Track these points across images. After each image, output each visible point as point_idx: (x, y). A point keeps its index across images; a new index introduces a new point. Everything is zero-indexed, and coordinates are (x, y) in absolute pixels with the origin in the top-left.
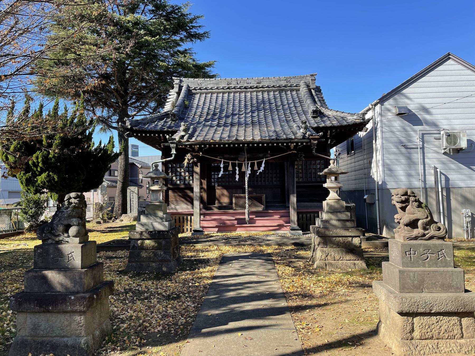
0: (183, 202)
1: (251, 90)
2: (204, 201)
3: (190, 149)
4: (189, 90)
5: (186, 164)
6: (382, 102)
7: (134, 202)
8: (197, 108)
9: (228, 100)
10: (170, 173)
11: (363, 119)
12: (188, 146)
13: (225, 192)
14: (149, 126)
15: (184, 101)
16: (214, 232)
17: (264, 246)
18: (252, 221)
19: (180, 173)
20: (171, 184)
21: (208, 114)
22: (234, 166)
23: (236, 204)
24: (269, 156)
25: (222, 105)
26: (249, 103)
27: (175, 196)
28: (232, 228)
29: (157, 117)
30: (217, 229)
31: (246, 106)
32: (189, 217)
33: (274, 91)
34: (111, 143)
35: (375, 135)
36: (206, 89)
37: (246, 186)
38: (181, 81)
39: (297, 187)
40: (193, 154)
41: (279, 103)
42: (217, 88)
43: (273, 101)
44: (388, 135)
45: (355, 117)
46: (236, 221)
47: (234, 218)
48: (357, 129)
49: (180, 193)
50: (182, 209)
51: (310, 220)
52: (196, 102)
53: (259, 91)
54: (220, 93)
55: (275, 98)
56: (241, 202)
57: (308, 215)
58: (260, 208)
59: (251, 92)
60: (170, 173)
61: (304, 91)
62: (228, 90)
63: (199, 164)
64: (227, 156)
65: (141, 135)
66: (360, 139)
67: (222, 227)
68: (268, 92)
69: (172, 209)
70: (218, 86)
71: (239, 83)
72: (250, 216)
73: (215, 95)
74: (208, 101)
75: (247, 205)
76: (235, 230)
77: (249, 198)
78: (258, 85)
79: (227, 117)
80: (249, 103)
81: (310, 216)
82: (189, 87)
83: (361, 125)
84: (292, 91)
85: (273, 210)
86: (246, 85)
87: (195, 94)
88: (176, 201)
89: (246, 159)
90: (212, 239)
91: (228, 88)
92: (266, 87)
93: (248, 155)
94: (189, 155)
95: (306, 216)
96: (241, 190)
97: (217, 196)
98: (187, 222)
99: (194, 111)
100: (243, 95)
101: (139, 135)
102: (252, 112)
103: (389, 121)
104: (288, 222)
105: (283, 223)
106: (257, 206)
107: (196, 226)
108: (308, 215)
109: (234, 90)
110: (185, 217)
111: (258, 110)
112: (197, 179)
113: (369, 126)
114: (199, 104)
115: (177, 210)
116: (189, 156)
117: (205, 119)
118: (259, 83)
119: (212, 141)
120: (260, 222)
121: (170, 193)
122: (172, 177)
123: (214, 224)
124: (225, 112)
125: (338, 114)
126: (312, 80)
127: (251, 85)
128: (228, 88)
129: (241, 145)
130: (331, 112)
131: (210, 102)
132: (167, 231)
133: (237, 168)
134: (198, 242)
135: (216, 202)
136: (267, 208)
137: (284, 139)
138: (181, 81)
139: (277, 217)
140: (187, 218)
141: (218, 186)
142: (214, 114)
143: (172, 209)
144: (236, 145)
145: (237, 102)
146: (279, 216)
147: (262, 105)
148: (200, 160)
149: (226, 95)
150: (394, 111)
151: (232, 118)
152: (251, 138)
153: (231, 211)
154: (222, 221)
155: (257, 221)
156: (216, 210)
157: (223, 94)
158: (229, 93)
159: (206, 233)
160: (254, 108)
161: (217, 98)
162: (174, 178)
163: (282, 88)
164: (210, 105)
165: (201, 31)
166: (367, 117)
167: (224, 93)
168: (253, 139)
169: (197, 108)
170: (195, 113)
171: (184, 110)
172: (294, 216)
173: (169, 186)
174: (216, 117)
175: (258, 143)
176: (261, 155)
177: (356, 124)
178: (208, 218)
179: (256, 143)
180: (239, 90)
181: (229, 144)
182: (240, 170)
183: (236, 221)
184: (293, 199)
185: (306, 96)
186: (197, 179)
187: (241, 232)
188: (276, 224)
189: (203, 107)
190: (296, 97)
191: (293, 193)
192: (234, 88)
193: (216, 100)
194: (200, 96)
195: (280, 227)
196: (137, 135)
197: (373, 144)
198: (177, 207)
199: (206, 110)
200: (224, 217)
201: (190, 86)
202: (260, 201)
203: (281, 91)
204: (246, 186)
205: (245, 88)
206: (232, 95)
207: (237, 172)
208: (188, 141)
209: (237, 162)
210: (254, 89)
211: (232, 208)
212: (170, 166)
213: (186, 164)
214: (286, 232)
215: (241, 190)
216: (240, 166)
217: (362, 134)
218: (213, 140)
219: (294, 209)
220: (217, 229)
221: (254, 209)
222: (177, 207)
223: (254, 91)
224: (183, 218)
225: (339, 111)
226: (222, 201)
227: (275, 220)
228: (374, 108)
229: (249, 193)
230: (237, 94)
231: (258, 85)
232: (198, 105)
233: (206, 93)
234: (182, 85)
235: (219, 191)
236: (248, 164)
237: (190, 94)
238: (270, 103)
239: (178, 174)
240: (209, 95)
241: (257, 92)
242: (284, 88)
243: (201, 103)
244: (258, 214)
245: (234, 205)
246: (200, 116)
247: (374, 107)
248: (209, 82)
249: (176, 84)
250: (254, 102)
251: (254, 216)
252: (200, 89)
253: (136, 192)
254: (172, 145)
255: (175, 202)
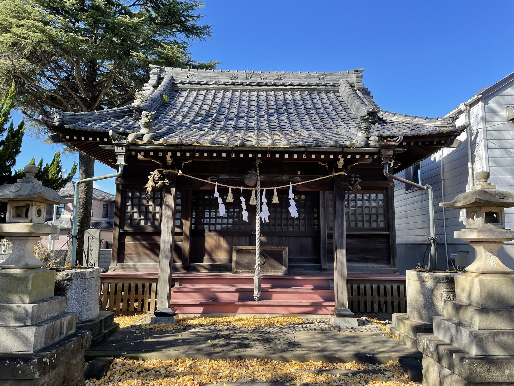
0: (149, 256)
1: (266, 87)
2: (184, 255)
3: (156, 158)
4: (173, 83)
5: (149, 189)
6: (485, 98)
7: (94, 252)
8: (181, 107)
9: (232, 100)
10: (129, 208)
11: (453, 126)
12: (151, 154)
13: (223, 242)
14: (93, 125)
15: (161, 96)
16: (194, 317)
17: (294, 362)
18: (265, 295)
19: (147, 207)
20: (131, 225)
21: (198, 114)
22: (236, 194)
23: (237, 263)
24: (299, 179)
25: (221, 105)
26: (263, 105)
27: (136, 247)
28: (230, 308)
29: (112, 113)
30: (201, 310)
31: (259, 107)
32: (154, 285)
33: (301, 91)
34: (55, 163)
35: (472, 153)
36: (199, 83)
37: (257, 233)
38: (162, 71)
39: (348, 236)
40: (164, 171)
41: (310, 106)
42: (216, 83)
43: (300, 103)
44: (497, 152)
45: (438, 123)
46: (237, 295)
47: (233, 289)
48: (443, 142)
49: (145, 240)
50: (147, 268)
51: (365, 295)
52: (182, 99)
53: (279, 90)
54: (220, 90)
55: (303, 100)
56: (246, 259)
57: (362, 286)
58: (280, 271)
59: (267, 91)
60: (129, 208)
61: (348, 90)
62: (232, 86)
63: (173, 190)
64: (223, 177)
65: (79, 139)
66: (437, 166)
67: (212, 305)
68: (293, 91)
69: (129, 267)
70: (217, 80)
71: (248, 77)
72: (263, 286)
73: (212, 93)
74: (200, 99)
75: (257, 267)
76: (234, 312)
77: (261, 254)
78: (277, 81)
79: (228, 119)
80: (263, 105)
81: (365, 287)
82: (174, 80)
83: (446, 138)
84: (327, 91)
85: (300, 275)
86: (259, 81)
87: (182, 90)
88: (138, 254)
89: (259, 183)
90: (184, 335)
91: (233, 84)
92: (289, 85)
93: (262, 177)
94: (156, 172)
95: (359, 287)
96: (247, 239)
97: (207, 246)
98: (150, 294)
99: (177, 108)
100: (254, 94)
101: (75, 138)
102: (269, 115)
103: (498, 130)
104: (331, 299)
105: (321, 300)
106: (273, 267)
107: (163, 307)
108: (362, 286)
109: (241, 86)
110: (147, 285)
111: (278, 111)
112: (168, 217)
113: (462, 137)
114: (186, 103)
115: (137, 271)
116: (155, 174)
117: (193, 120)
118: (278, 79)
119: (196, 144)
120: (279, 297)
121: (128, 240)
122: (133, 213)
123: (197, 299)
124: (225, 115)
125: (408, 119)
126: (357, 77)
127: (267, 81)
128: (233, 84)
129: (251, 155)
130: (396, 117)
131: (203, 101)
132: (26, 358)
133: (242, 199)
134: (152, 348)
135: (206, 257)
136: (291, 271)
137: (331, 146)
138: (162, 71)
139: (308, 288)
140: (150, 286)
141: (210, 231)
142: (208, 115)
143: (129, 267)
144: (242, 155)
145: (245, 103)
146: (312, 287)
147: (284, 108)
148: (176, 181)
149: (229, 94)
150: (505, 115)
151: (237, 121)
152: (270, 142)
153: (229, 275)
154: (211, 295)
155: (274, 296)
156: (204, 273)
157: (224, 91)
158: (234, 90)
159: (181, 316)
160: (272, 111)
161: (214, 96)
162: (136, 216)
163: (313, 87)
164: (202, 104)
165: (199, 24)
166: (459, 123)
167: (225, 90)
168: (273, 143)
169: (181, 107)
170: (178, 112)
171: (161, 109)
172: (341, 291)
173: (126, 229)
174: (210, 118)
175: (282, 152)
176: (285, 178)
177: (442, 133)
178: (188, 286)
179: (277, 152)
180: (249, 87)
181: (229, 152)
182: (247, 202)
183: (237, 295)
184: (341, 256)
185: (352, 96)
186: (168, 217)
187: (244, 318)
188: (308, 302)
189: (191, 106)
190: (335, 99)
191: (342, 248)
192: (242, 84)
193: (213, 99)
194: (189, 93)
195: (316, 307)
196: (71, 139)
197: (468, 168)
198: (139, 265)
199: (196, 108)
200: (216, 287)
201: (175, 78)
202: (278, 257)
203: (311, 92)
204: (257, 233)
205: (258, 85)
206: (238, 93)
207: (244, 205)
208: (150, 142)
209: (242, 188)
210: (271, 87)
211: (230, 270)
212: (130, 194)
213: (149, 189)
214: (327, 318)
215: (247, 239)
216: (248, 195)
217: (442, 154)
218: (198, 143)
219: (342, 276)
220: (201, 310)
221: (270, 273)
222: (139, 265)
223: (271, 90)
224: (143, 286)
225: (401, 121)
226: (214, 257)
227: (305, 294)
228: (469, 111)
229: (261, 243)
230: (246, 93)
231: (277, 81)
232: (184, 103)
233: (199, 90)
234: (162, 76)
235: (211, 241)
236: (262, 191)
237: (174, 89)
238: (296, 105)
239: (143, 208)
240: (203, 93)
241: (275, 91)
242: (316, 87)
243: (190, 101)
244: (277, 282)
245: (234, 265)
246: (185, 117)
247: (468, 108)
248: (204, 75)
249: (154, 74)
250: (272, 103)
251: (269, 286)
252: (190, 83)
253: (97, 236)
254: (118, 149)
255: (136, 259)
